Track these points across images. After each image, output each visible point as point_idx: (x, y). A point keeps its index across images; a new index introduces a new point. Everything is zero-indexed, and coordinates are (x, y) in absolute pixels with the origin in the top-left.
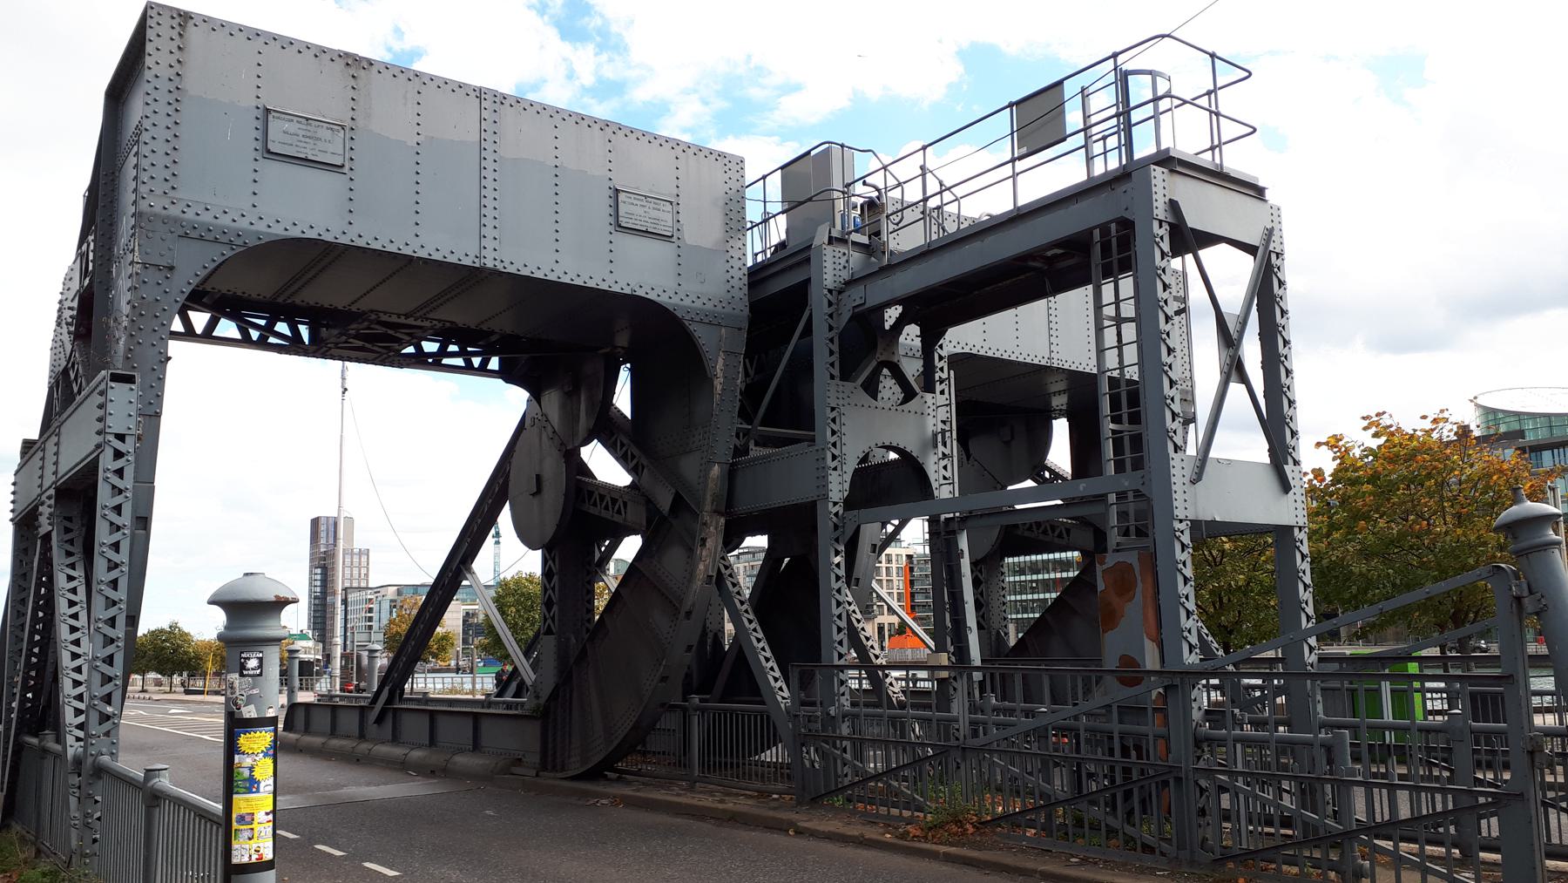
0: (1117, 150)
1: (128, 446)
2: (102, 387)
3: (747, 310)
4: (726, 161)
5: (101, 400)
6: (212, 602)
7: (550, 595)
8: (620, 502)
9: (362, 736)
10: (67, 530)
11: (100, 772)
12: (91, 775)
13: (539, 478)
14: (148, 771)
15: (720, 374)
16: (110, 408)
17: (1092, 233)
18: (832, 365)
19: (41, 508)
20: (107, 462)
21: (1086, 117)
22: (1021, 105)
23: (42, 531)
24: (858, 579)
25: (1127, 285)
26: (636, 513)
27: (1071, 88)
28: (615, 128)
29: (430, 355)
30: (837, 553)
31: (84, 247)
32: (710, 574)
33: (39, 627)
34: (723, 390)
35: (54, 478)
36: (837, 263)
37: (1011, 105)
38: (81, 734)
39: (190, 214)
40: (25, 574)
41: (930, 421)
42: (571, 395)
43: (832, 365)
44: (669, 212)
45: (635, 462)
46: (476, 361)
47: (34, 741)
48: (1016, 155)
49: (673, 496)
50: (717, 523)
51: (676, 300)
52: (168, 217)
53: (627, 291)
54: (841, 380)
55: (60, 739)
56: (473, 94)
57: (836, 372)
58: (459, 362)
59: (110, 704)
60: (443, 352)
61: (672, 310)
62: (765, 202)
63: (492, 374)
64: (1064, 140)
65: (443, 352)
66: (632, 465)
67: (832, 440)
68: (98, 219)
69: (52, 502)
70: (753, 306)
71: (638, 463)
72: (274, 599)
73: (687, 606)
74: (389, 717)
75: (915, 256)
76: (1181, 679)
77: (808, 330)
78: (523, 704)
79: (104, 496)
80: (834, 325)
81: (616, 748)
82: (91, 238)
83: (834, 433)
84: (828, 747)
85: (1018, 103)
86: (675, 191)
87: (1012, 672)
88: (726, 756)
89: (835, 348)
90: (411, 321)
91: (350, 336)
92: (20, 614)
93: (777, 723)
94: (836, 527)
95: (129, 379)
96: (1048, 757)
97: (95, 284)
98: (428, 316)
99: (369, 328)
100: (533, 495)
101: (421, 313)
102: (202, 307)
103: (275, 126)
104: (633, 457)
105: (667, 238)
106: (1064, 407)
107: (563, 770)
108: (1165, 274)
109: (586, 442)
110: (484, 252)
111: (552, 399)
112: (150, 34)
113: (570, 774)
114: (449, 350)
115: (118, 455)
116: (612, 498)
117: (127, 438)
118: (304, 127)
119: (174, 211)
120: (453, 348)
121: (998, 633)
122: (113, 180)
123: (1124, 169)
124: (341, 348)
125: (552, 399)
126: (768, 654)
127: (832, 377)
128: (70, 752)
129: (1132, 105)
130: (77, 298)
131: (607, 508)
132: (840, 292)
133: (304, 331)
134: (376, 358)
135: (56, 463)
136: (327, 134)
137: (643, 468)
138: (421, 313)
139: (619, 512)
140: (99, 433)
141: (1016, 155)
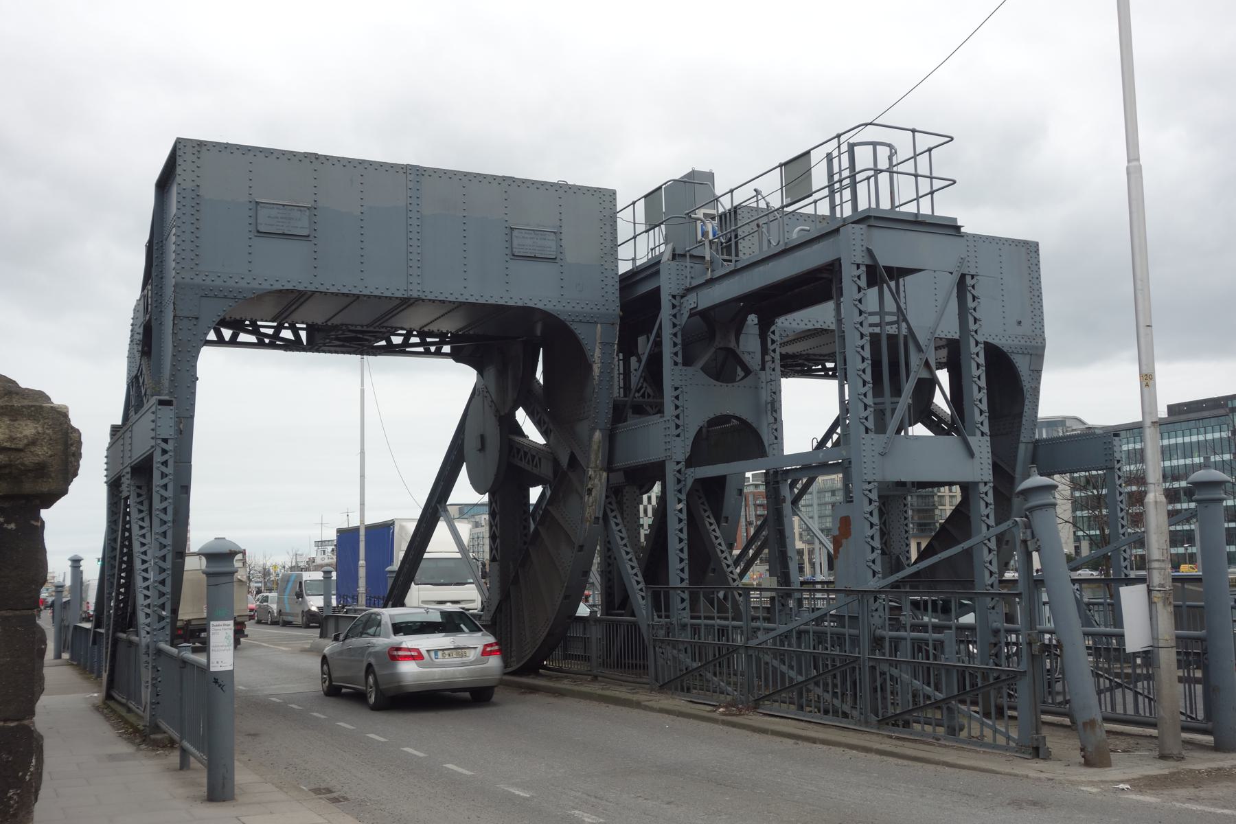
0: (844, 201)
2: (153, 409)
3: (618, 310)
4: (601, 195)
5: (153, 417)
7: (494, 531)
8: (537, 459)
10: (139, 495)
12: (155, 654)
20: (158, 458)
22: (788, 166)
23: (124, 494)
24: (727, 518)
26: (546, 469)
29: (397, 346)
31: (146, 291)
32: (597, 515)
33: (125, 559)
34: (601, 372)
36: (680, 275)
37: (781, 165)
38: (148, 629)
39: (208, 282)
40: (115, 521)
44: (553, 240)
45: (546, 426)
46: (433, 349)
47: (174, 651)
48: (784, 204)
49: (569, 455)
50: (601, 476)
53: (520, 304)
54: (683, 365)
56: (401, 171)
57: (679, 360)
58: (421, 349)
61: (556, 315)
62: (634, 224)
63: (446, 355)
64: (811, 195)
65: (406, 343)
66: (544, 428)
70: (624, 306)
71: (547, 428)
72: (228, 552)
75: (727, 273)
76: (862, 596)
79: (157, 480)
80: (678, 323)
81: (537, 651)
82: (149, 287)
84: (907, 677)
85: (786, 164)
86: (558, 224)
87: (659, 589)
88: (628, 658)
90: (371, 329)
91: (332, 339)
92: (114, 549)
93: (641, 627)
95: (169, 403)
96: (776, 651)
97: (153, 321)
98: (384, 325)
100: (480, 450)
101: (377, 324)
102: (228, 326)
104: (545, 423)
106: (945, 360)
108: (861, 303)
111: (491, 372)
114: (411, 341)
115: (164, 452)
116: (532, 455)
117: (169, 441)
119: (198, 280)
121: (898, 557)
122: (162, 246)
123: (844, 221)
124: (328, 346)
127: (676, 364)
129: (857, 170)
130: (142, 327)
132: (682, 297)
133: (303, 334)
134: (356, 351)
137: (551, 431)
138: (377, 324)
139: (536, 466)
141: (784, 204)
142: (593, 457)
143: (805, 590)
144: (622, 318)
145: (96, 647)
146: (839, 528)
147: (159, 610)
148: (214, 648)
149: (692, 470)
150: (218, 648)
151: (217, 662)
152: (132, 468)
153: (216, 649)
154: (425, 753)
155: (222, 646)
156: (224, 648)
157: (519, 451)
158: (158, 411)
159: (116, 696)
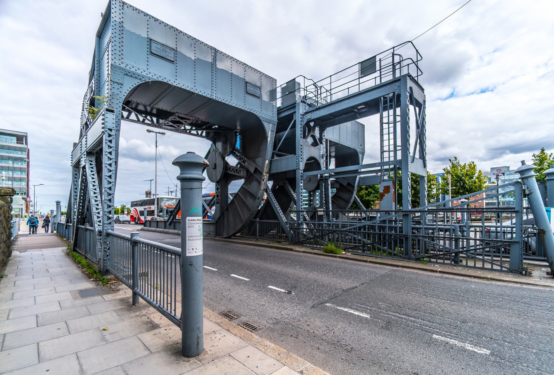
1: (113, 133)
2: (104, 113)
6: (175, 163)
9: (165, 228)
11: (108, 235)
13: (215, 165)
14: (132, 234)
15: (270, 136)
16: (106, 120)
17: (381, 98)
18: (301, 134)
19: (81, 159)
20: (105, 137)
21: (380, 67)
25: (398, 110)
27: (378, 59)
28: (246, 65)
30: (301, 183)
35: (86, 149)
37: (359, 63)
39: (128, 68)
41: (322, 151)
42: (225, 143)
43: (301, 128)
45: (243, 160)
47: (83, 227)
51: (260, 115)
52: (121, 67)
53: (249, 111)
55: (92, 225)
56: (210, 48)
57: (302, 136)
59: (111, 214)
60: (191, 129)
63: (203, 137)
67: (301, 154)
68: (95, 74)
69: (85, 156)
73: (259, 196)
74: (173, 223)
77: (294, 126)
78: (210, 220)
83: (301, 152)
85: (361, 63)
89: (302, 130)
91: (169, 121)
94: (301, 176)
95: (112, 111)
99: (174, 119)
100: (214, 169)
103: (154, 45)
104: (242, 159)
105: (259, 98)
107: (222, 236)
109: (229, 155)
110: (213, 94)
111: (219, 145)
112: (112, 6)
113: (224, 237)
115: (110, 136)
118: (162, 47)
119: (123, 66)
120: (194, 128)
125: (219, 145)
126: (280, 208)
127: (301, 137)
128: (97, 229)
131: (234, 172)
135: (86, 144)
136: (169, 51)
139: (238, 173)
140: (103, 128)
142: (265, 168)
143: (417, 212)
144: (278, 123)
145: (67, 230)
146: (383, 190)
147: (108, 215)
148: (190, 238)
149: (307, 173)
150: (194, 238)
151: (193, 249)
152: (87, 152)
153: (192, 239)
154: (269, 288)
155: (196, 236)
156: (197, 238)
157: (230, 168)
158: (106, 114)
159: (77, 249)
